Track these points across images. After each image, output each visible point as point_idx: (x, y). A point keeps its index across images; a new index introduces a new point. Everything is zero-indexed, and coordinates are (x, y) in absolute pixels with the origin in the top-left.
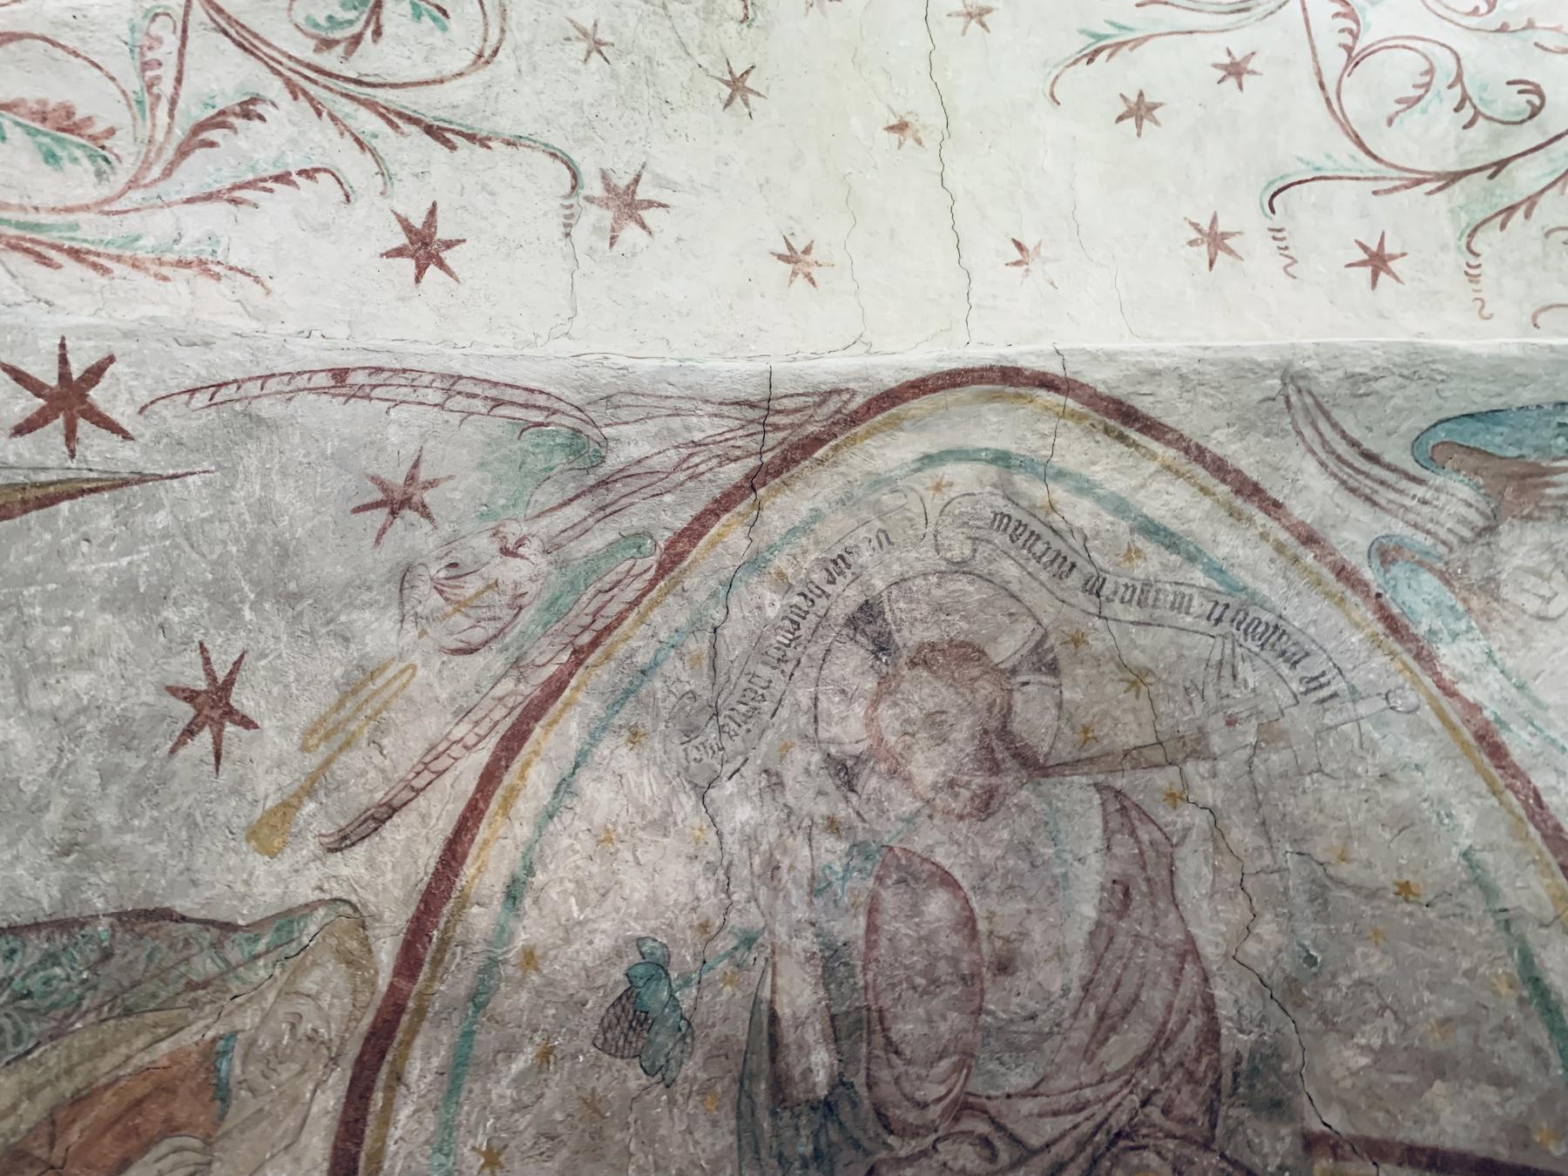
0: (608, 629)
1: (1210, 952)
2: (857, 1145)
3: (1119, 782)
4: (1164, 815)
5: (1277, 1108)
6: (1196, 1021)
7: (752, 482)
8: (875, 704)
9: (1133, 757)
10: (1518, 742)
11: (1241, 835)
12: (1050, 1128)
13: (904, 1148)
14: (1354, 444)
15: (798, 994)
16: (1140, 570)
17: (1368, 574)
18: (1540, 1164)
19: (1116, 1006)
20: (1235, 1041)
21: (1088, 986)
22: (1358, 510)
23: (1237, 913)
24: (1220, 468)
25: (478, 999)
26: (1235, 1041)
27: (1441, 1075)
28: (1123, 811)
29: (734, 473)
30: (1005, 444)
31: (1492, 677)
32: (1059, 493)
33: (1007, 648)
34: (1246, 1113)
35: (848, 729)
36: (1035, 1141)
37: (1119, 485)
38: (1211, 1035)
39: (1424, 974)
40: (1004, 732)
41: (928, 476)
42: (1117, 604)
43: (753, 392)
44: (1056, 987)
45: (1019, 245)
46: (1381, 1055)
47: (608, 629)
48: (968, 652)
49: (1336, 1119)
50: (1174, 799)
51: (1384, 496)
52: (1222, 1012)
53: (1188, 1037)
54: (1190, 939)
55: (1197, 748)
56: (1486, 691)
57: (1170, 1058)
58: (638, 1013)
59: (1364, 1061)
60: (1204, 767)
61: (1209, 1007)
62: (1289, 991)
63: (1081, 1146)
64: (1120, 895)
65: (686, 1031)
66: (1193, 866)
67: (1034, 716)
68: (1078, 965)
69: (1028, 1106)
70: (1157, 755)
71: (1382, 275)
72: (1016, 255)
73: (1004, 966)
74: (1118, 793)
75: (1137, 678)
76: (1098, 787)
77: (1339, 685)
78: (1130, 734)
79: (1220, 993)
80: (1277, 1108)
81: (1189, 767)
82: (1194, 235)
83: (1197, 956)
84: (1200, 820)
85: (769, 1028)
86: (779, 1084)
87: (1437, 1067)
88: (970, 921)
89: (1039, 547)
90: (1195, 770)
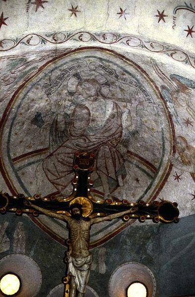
0: (30, 79)
1: (124, 127)
2: (66, 136)
3: (117, 102)
4: (122, 108)
5: (126, 146)
6: (119, 134)
7: (54, 59)
8: (78, 85)
9: (119, 99)
10: (174, 118)
11: (133, 114)
12: (95, 140)
13: (73, 138)
14: (161, 71)
15: (60, 118)
16: (124, 77)
17: (160, 89)
18: (194, 155)
19: (108, 129)
20: (123, 137)
21: (105, 126)
22: (161, 80)
23: (129, 123)
24: (139, 67)
25: (14, 119)
26: (123, 137)
27: (147, 150)
28: (116, 106)
29: (51, 59)
30: (101, 57)
31: (173, 109)
32: (111, 64)
33: (102, 81)
34: (121, 145)
35: (73, 88)
36: (92, 141)
37: (122, 65)
38: (121, 136)
39: (151, 139)
40: (100, 91)
41: (86, 59)
42: (120, 80)
43: (55, 49)
44: (100, 125)
45: (121, 10)
46: (141, 145)
47: (30, 79)
48: (94, 81)
49: (132, 150)
50: (125, 107)
51: (165, 80)
52: (123, 134)
53: (117, 136)
54: (121, 124)
55: (130, 101)
56: (172, 110)
57: (114, 137)
58: (37, 119)
59: (139, 145)
60: (130, 104)
61: (122, 132)
62: (135, 133)
63: (98, 143)
64: (113, 116)
65: (43, 122)
66: (125, 116)
67: (105, 90)
68: (104, 123)
69: (92, 137)
70: (124, 101)
71: (189, 35)
72: (120, 11)
73: (93, 120)
74: (116, 104)
75: (122, 90)
76: (113, 102)
77: (152, 101)
78: (120, 96)
79: (123, 131)
80: (126, 146)
81: (128, 103)
82: (158, 14)
83: (122, 126)
84: (127, 111)
85: (56, 122)
86: (56, 129)
87: (147, 149)
88: (90, 114)
89: (107, 70)
90: (129, 104)
